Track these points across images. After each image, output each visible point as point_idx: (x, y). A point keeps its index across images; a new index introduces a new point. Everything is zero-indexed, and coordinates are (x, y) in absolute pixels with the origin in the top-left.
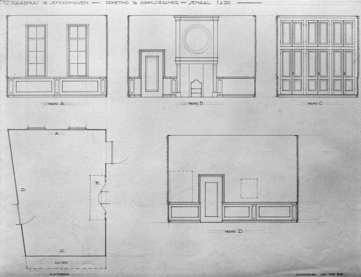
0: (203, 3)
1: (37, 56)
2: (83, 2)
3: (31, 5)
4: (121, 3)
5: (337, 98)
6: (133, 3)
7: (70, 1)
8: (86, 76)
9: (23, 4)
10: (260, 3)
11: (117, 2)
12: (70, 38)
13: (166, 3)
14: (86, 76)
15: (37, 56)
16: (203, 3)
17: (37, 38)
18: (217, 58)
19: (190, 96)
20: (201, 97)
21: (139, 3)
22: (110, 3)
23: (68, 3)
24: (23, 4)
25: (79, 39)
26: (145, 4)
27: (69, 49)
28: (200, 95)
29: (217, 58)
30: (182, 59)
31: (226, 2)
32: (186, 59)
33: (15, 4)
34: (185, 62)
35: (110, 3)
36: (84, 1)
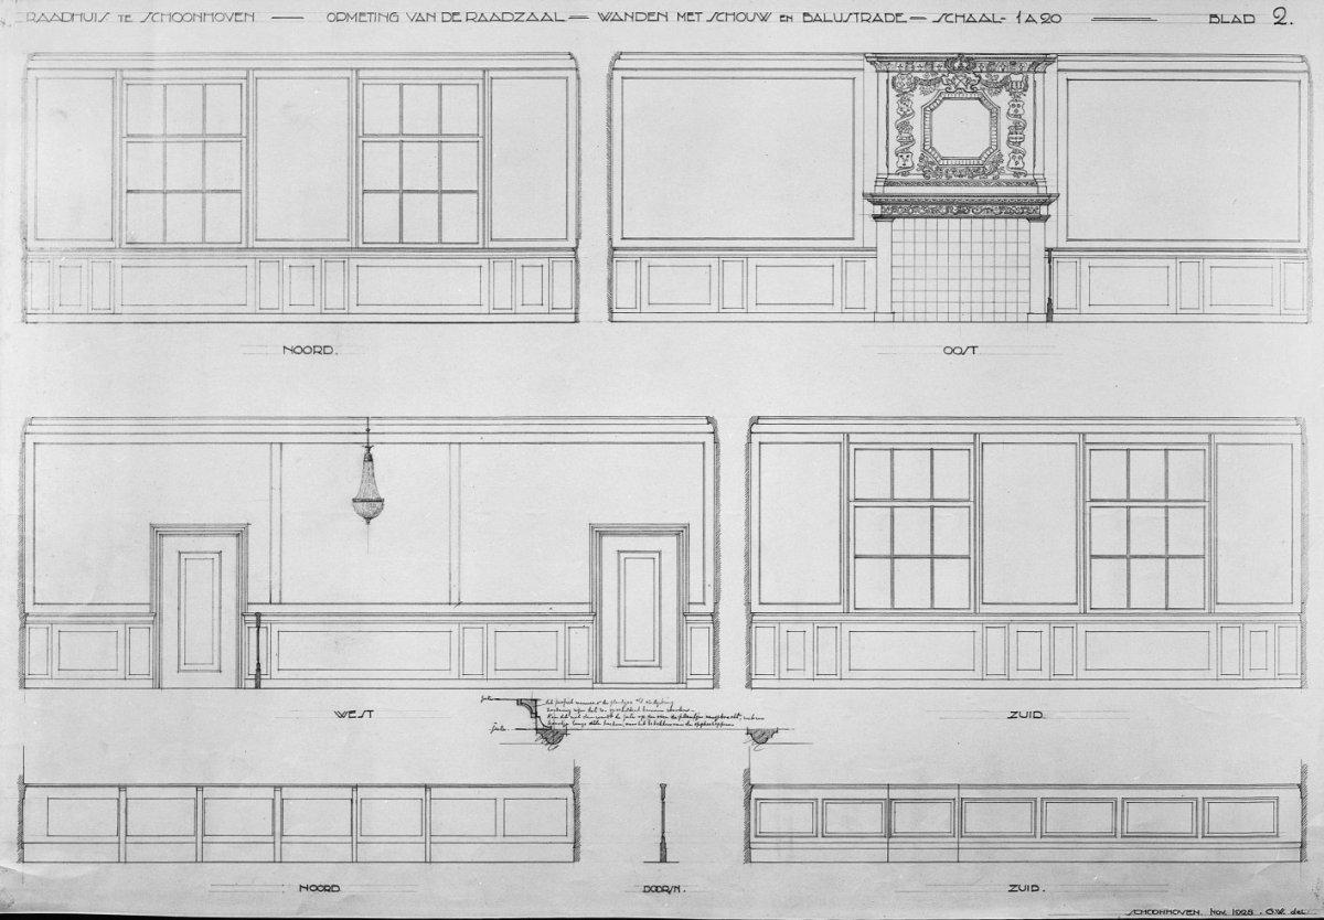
0: (540, 17)
8: (1300, 786)
9: (881, 20)
10: (1149, 19)
11: (690, 14)
12: (856, 500)
13: (616, 18)
14: (1300, 786)
16: (540, 17)
17: (1132, 497)
18: (1167, 606)
19: (122, 860)
20: (196, 862)
22: (341, 17)
24: (881, 20)
25: (1169, 504)
27: (883, 612)
28: (344, 852)
29: (1167, 606)
31: (1047, 16)
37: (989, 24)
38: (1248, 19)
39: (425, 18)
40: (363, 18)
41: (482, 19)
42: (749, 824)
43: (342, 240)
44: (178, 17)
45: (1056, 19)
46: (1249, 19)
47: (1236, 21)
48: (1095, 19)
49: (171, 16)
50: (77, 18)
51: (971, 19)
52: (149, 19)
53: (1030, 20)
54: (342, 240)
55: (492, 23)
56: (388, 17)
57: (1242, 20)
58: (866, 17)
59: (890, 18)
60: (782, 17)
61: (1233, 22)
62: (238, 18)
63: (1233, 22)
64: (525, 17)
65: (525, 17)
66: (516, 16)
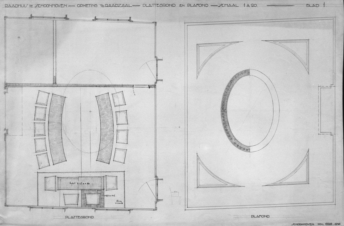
0: (232, 6)
1: (156, 169)
2: (87, 5)
3: (21, 8)
4: (90, 5)
5: (332, 149)
6: (101, 6)
7: (172, 4)
9: (151, 6)
11: (87, 5)
13: (314, 6)
15: (156, 169)
21: (99, 6)
22: (82, 5)
23: (203, 6)
24: (151, 6)
26: (162, 7)
30: (84, 175)
31: (253, 5)
32: (57, 186)
33: (8, 7)
34: (103, 182)
35: (82, 5)
36: (63, 4)
37: (115, 7)
38: (317, 6)
39: (196, 5)
40: (87, 6)
41: (110, 6)
42: (111, 209)
43: (334, 140)
44: (45, 6)
45: (255, 5)
46: (317, 6)
47: (314, 6)
48: (139, 6)
49: (44, 5)
50: (19, 6)
51: (230, 5)
52: (37, 6)
53: (248, 6)
54: (334, 140)
55: (233, 7)
56: (94, 6)
57: (105, 6)
58: (107, 5)
59: (117, 5)
60: (180, 5)
61: (257, 217)
62: (62, 6)
63: (257, 217)
64: (121, 6)
65: (121, 6)
66: (119, 5)
